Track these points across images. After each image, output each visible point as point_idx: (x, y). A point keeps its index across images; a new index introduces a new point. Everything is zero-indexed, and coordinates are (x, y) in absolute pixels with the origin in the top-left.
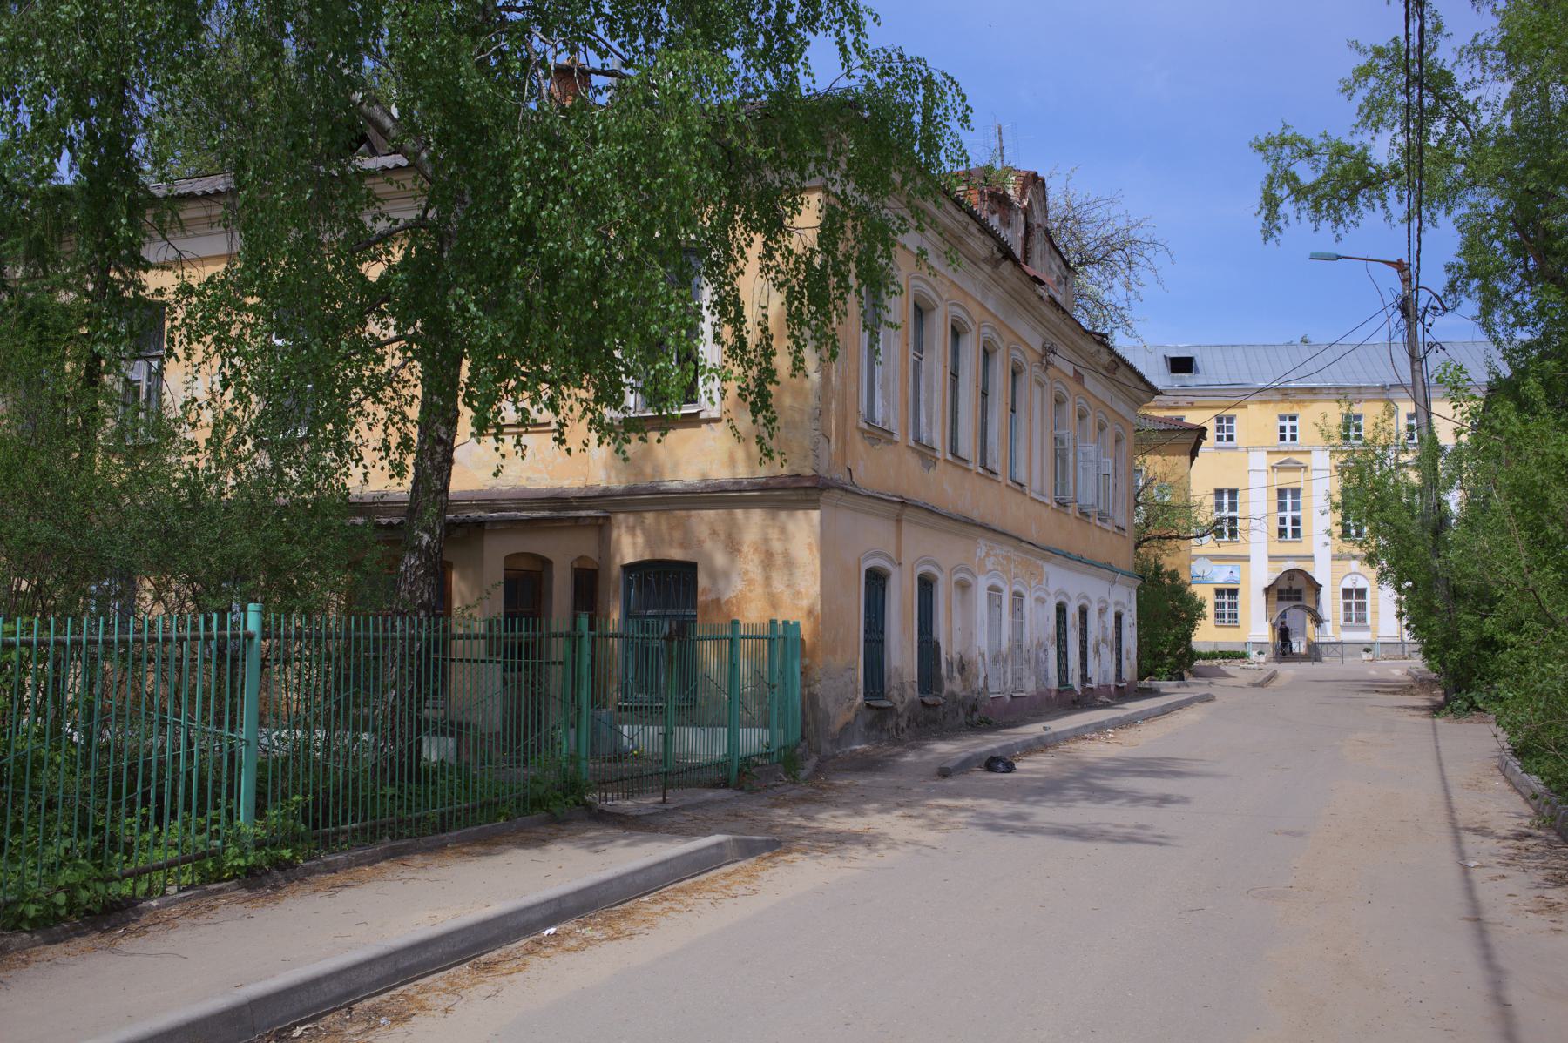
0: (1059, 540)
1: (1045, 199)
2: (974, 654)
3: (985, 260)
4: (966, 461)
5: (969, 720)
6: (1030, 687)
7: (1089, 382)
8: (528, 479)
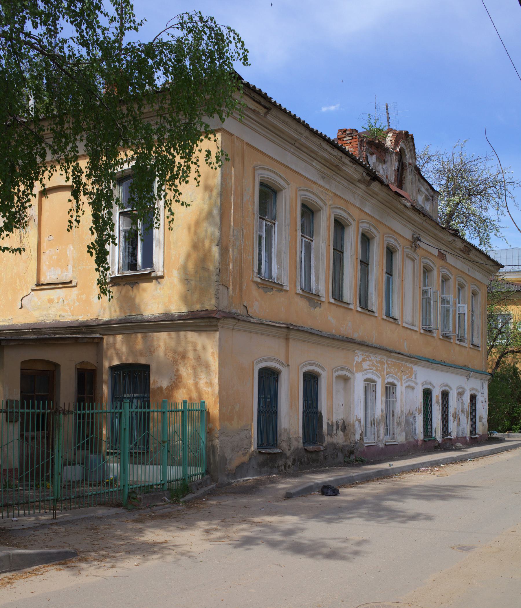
0: (427, 351)
1: (414, 148)
2: (352, 419)
3: (359, 181)
4: (347, 304)
5: (347, 459)
6: (401, 438)
7: (450, 259)
8: (60, 315)
